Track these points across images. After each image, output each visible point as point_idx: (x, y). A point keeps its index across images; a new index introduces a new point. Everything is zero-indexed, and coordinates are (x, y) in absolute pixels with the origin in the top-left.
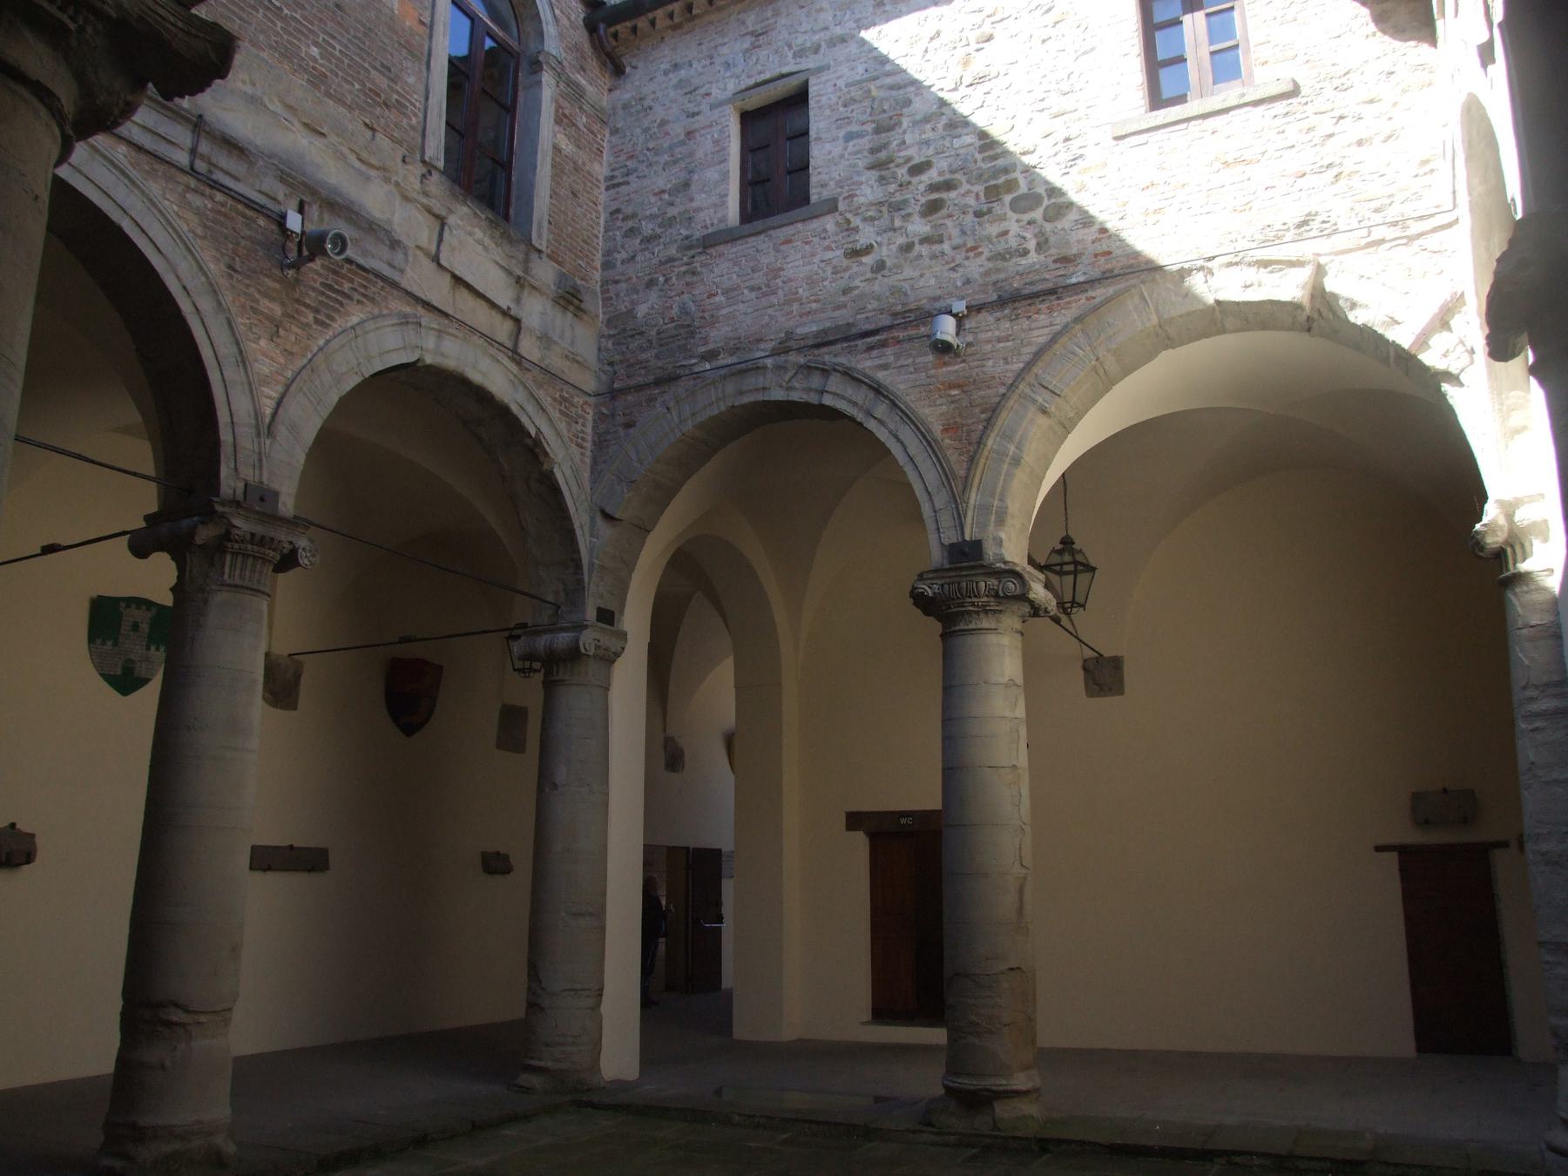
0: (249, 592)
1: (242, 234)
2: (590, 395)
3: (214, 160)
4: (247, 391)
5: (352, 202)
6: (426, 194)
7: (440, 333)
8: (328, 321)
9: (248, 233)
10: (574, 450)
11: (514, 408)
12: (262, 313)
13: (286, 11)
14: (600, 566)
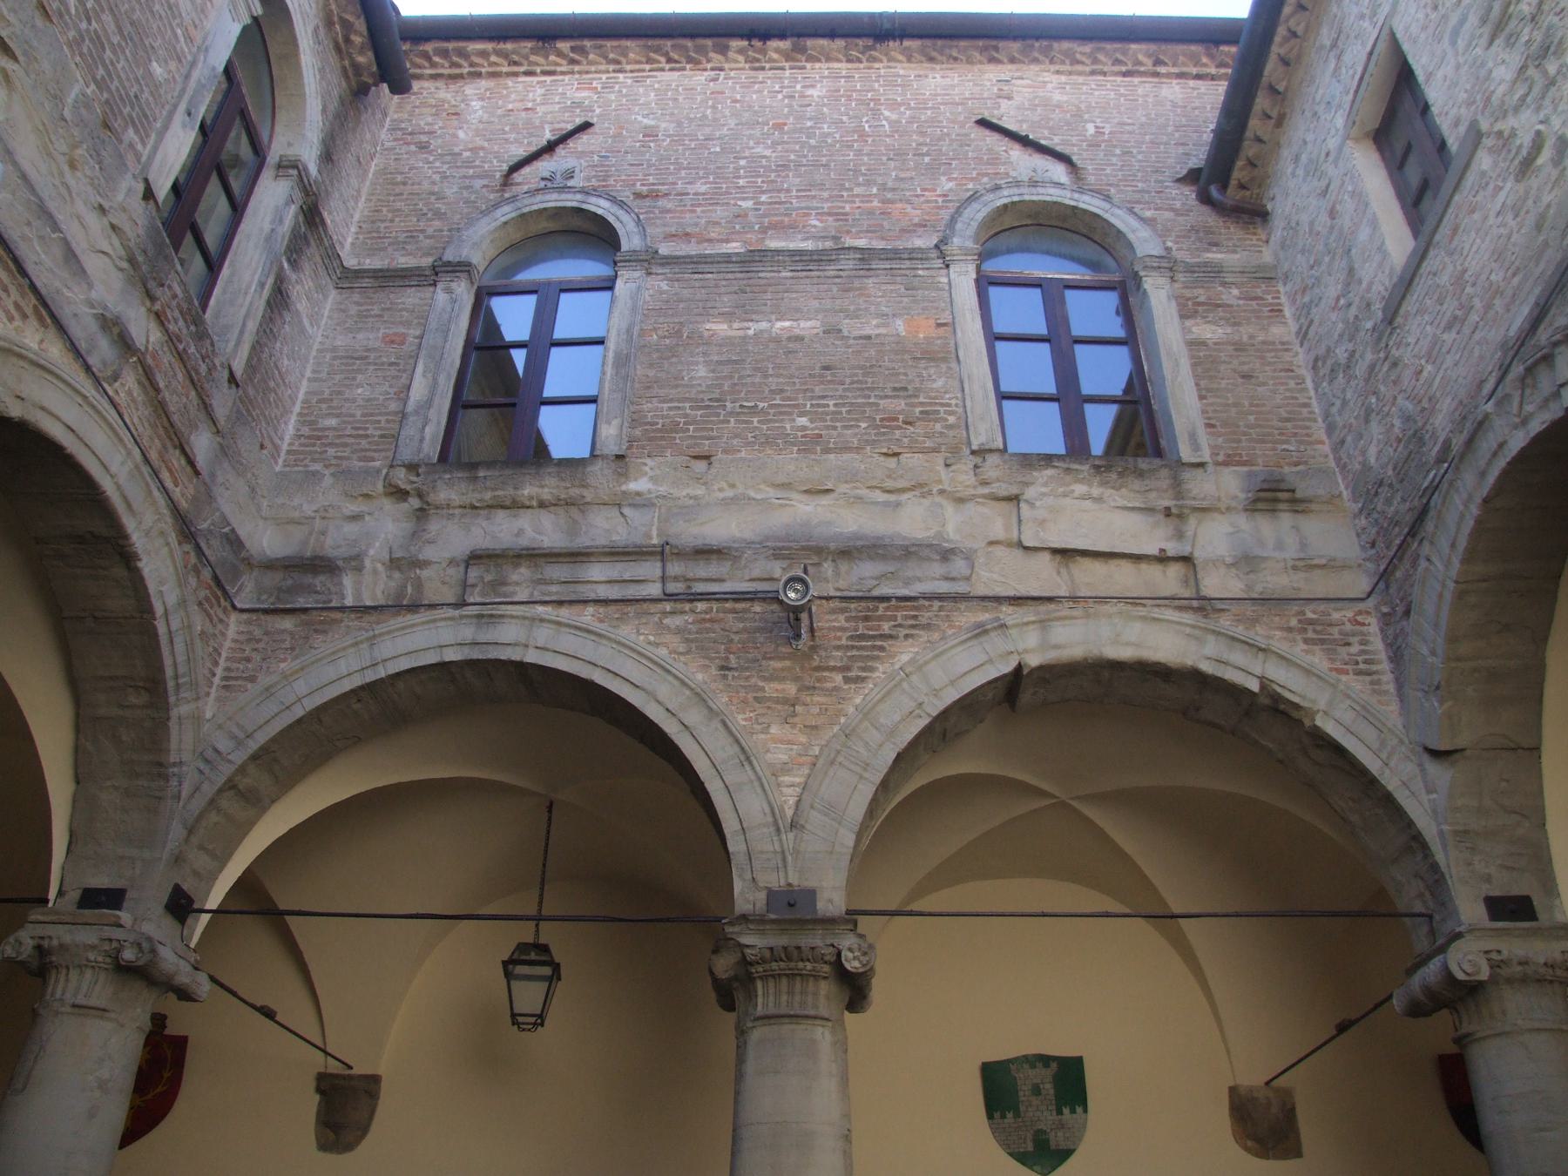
0: (787, 1020)
1: (734, 630)
2: (1362, 600)
3: (690, 575)
4: (759, 790)
5: (878, 538)
6: (985, 483)
7: (1043, 623)
8: (864, 674)
9: (741, 625)
10: (1357, 685)
11: (1206, 667)
12: (770, 699)
13: (761, 405)
14: (1456, 833)
